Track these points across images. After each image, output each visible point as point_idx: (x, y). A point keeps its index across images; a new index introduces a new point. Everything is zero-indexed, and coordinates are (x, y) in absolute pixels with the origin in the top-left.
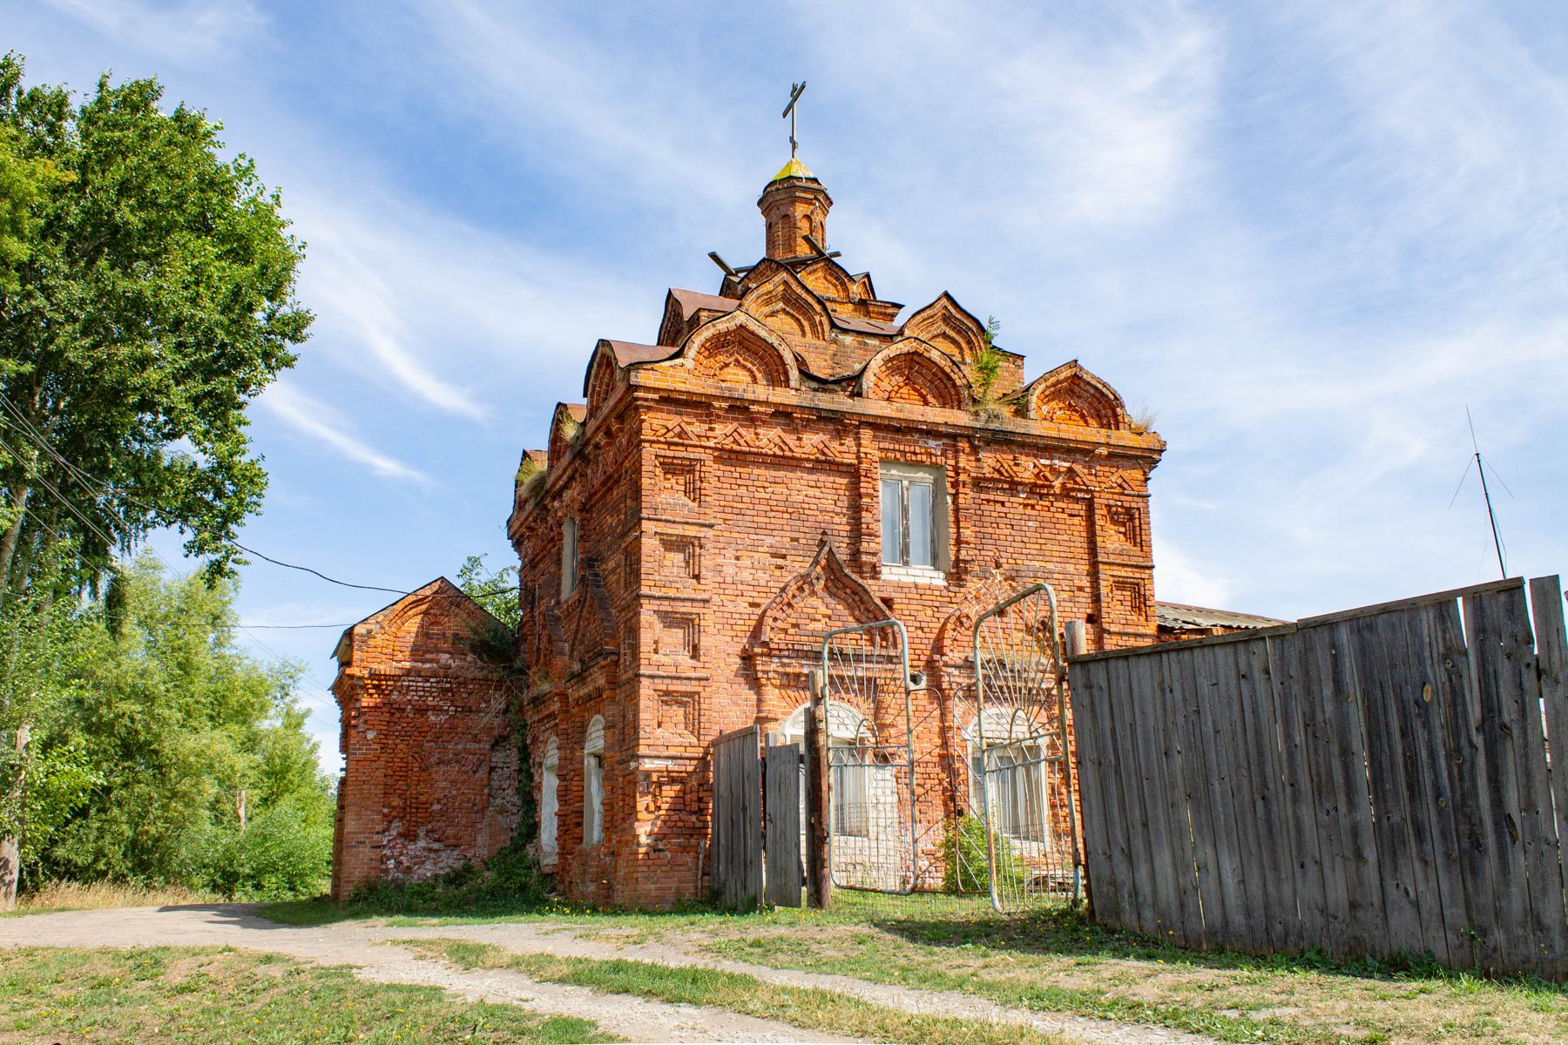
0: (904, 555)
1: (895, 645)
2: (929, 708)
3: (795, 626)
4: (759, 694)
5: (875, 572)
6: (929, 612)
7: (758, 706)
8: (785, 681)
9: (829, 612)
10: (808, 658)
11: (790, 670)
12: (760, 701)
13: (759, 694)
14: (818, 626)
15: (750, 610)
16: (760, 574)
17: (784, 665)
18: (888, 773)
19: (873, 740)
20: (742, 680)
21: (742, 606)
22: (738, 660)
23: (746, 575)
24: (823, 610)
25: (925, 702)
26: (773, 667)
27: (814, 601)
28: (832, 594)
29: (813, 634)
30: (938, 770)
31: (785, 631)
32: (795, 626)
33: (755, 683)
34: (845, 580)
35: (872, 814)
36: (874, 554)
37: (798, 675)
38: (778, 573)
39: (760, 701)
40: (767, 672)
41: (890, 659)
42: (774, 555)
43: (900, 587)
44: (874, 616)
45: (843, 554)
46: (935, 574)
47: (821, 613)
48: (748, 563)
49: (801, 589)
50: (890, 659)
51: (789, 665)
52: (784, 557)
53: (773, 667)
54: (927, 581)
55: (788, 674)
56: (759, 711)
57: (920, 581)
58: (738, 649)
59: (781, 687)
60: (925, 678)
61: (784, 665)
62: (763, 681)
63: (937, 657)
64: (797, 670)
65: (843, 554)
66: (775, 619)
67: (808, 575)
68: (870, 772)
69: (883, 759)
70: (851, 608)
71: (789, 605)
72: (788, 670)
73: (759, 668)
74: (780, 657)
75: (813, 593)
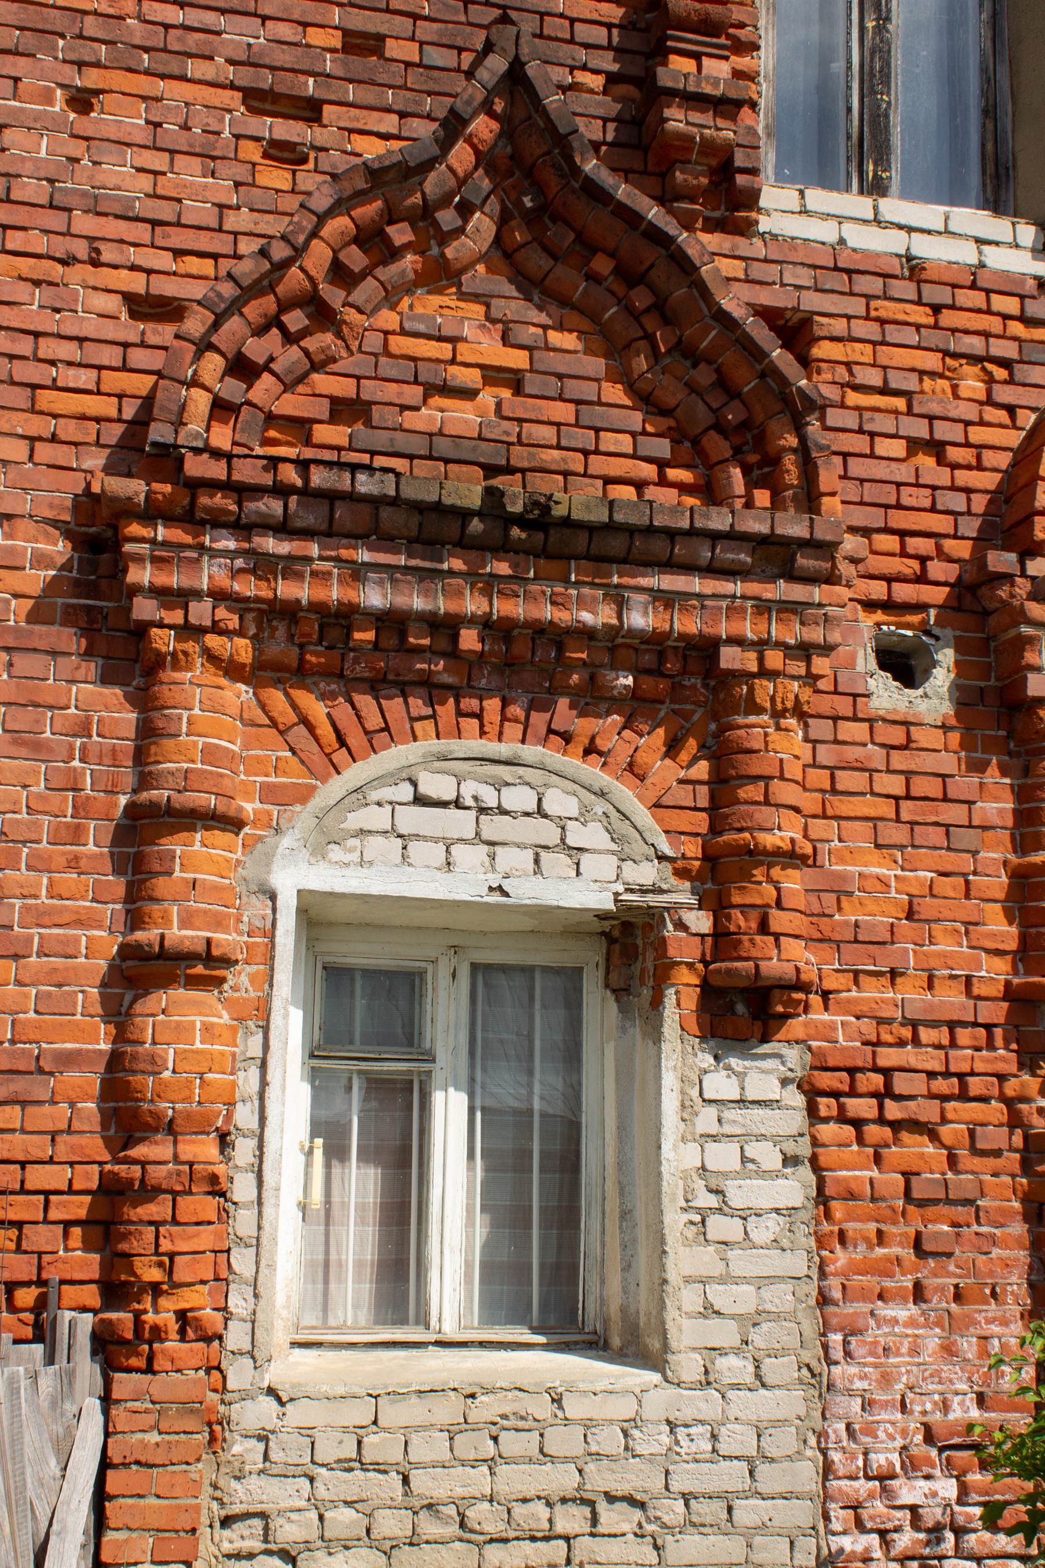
0: (862, 157)
1: (810, 500)
2: (964, 784)
3: (345, 410)
4: (145, 701)
5: (731, 202)
6: (972, 385)
7: (140, 756)
8: (279, 647)
9: (517, 359)
10: (385, 540)
11: (301, 592)
12: (149, 734)
13: (145, 701)
14: (463, 417)
15: (130, 330)
16: (189, 173)
17: (264, 566)
18: (766, 1075)
19: (701, 922)
20: (68, 638)
21: (95, 306)
22: (60, 548)
23: (121, 176)
24: (488, 348)
25: (948, 763)
26: (210, 574)
27: (430, 306)
28: (531, 286)
29: (436, 448)
30: (1004, 1058)
31: (300, 428)
32: (345, 410)
33: (129, 658)
34: (596, 221)
35: (684, 1259)
36: (848, 1354)
37: (341, 619)
38: (276, 177)
39: (149, 734)
40: (183, 597)
41: (776, 556)
42: (258, 100)
43: (843, 268)
44: (736, 398)
45: (583, 99)
46: (998, 227)
47: (474, 369)
48: (134, 122)
49: (372, 239)
50: (776, 556)
51: (291, 567)
52: (310, 111)
53: (210, 574)
54: (966, 254)
55: (287, 612)
56: (145, 781)
57: (930, 250)
58: (58, 495)
59: (259, 673)
60: (947, 656)
61: (264, 566)
62: (164, 640)
63: (1002, 560)
64: (335, 593)
65: (583, 99)
66: (242, 368)
67: (408, 172)
68: (680, 1059)
69: (743, 1011)
70: (613, 347)
71: (323, 316)
72: (286, 589)
73: (142, 575)
74: (242, 528)
75: (441, 275)
